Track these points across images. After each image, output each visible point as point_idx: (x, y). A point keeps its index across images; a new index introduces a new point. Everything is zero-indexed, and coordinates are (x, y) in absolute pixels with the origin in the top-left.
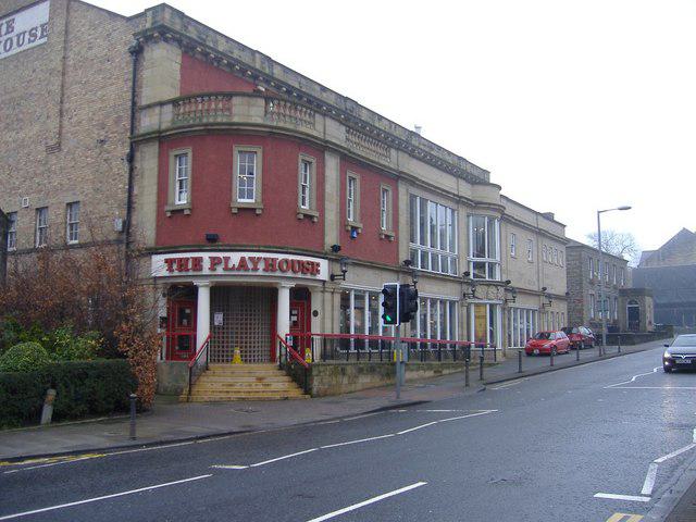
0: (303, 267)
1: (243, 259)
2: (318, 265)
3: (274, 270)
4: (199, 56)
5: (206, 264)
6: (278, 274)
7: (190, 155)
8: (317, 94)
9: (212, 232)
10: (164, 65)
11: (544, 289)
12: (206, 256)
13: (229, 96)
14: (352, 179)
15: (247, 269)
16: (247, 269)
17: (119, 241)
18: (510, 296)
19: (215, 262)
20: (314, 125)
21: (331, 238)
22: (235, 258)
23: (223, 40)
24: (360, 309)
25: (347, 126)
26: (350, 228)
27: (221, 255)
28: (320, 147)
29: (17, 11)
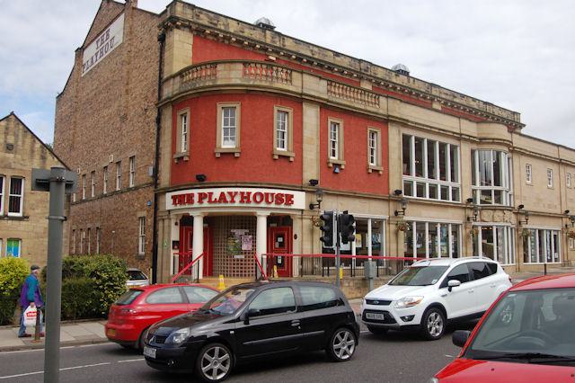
0: (279, 199)
1: (222, 194)
2: (292, 196)
3: (249, 201)
4: (211, 38)
5: (196, 198)
6: (253, 204)
7: (189, 114)
8: (330, 59)
9: (201, 174)
10: (182, 49)
11: (567, 212)
12: (196, 192)
13: (214, 64)
14: (335, 125)
15: (226, 201)
16: (226, 201)
17: (151, 184)
18: (523, 219)
19: (202, 197)
20: (291, 81)
21: (311, 171)
22: (217, 193)
23: (235, 23)
24: (445, 240)
25: (328, 80)
26: (331, 165)
27: (206, 191)
28: (298, 100)
29: (111, 23)
